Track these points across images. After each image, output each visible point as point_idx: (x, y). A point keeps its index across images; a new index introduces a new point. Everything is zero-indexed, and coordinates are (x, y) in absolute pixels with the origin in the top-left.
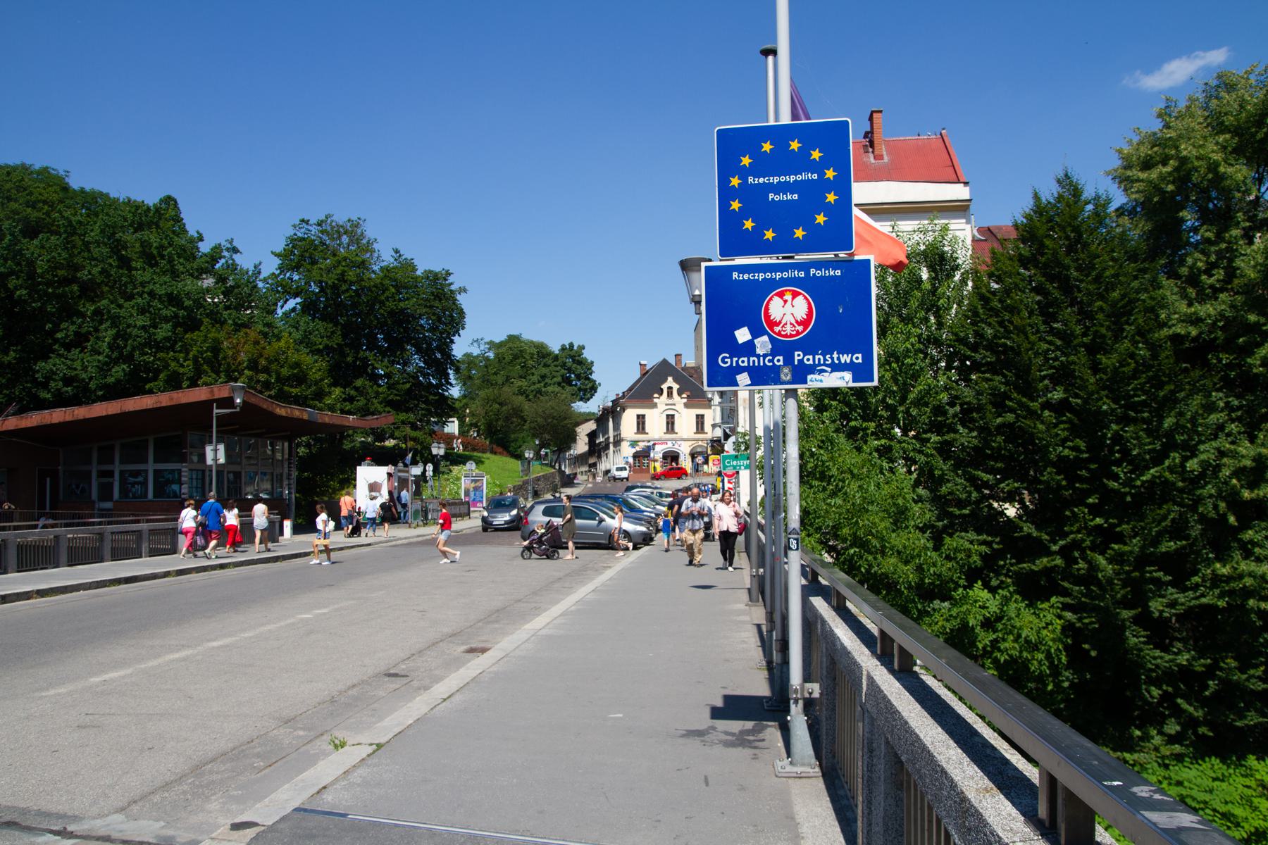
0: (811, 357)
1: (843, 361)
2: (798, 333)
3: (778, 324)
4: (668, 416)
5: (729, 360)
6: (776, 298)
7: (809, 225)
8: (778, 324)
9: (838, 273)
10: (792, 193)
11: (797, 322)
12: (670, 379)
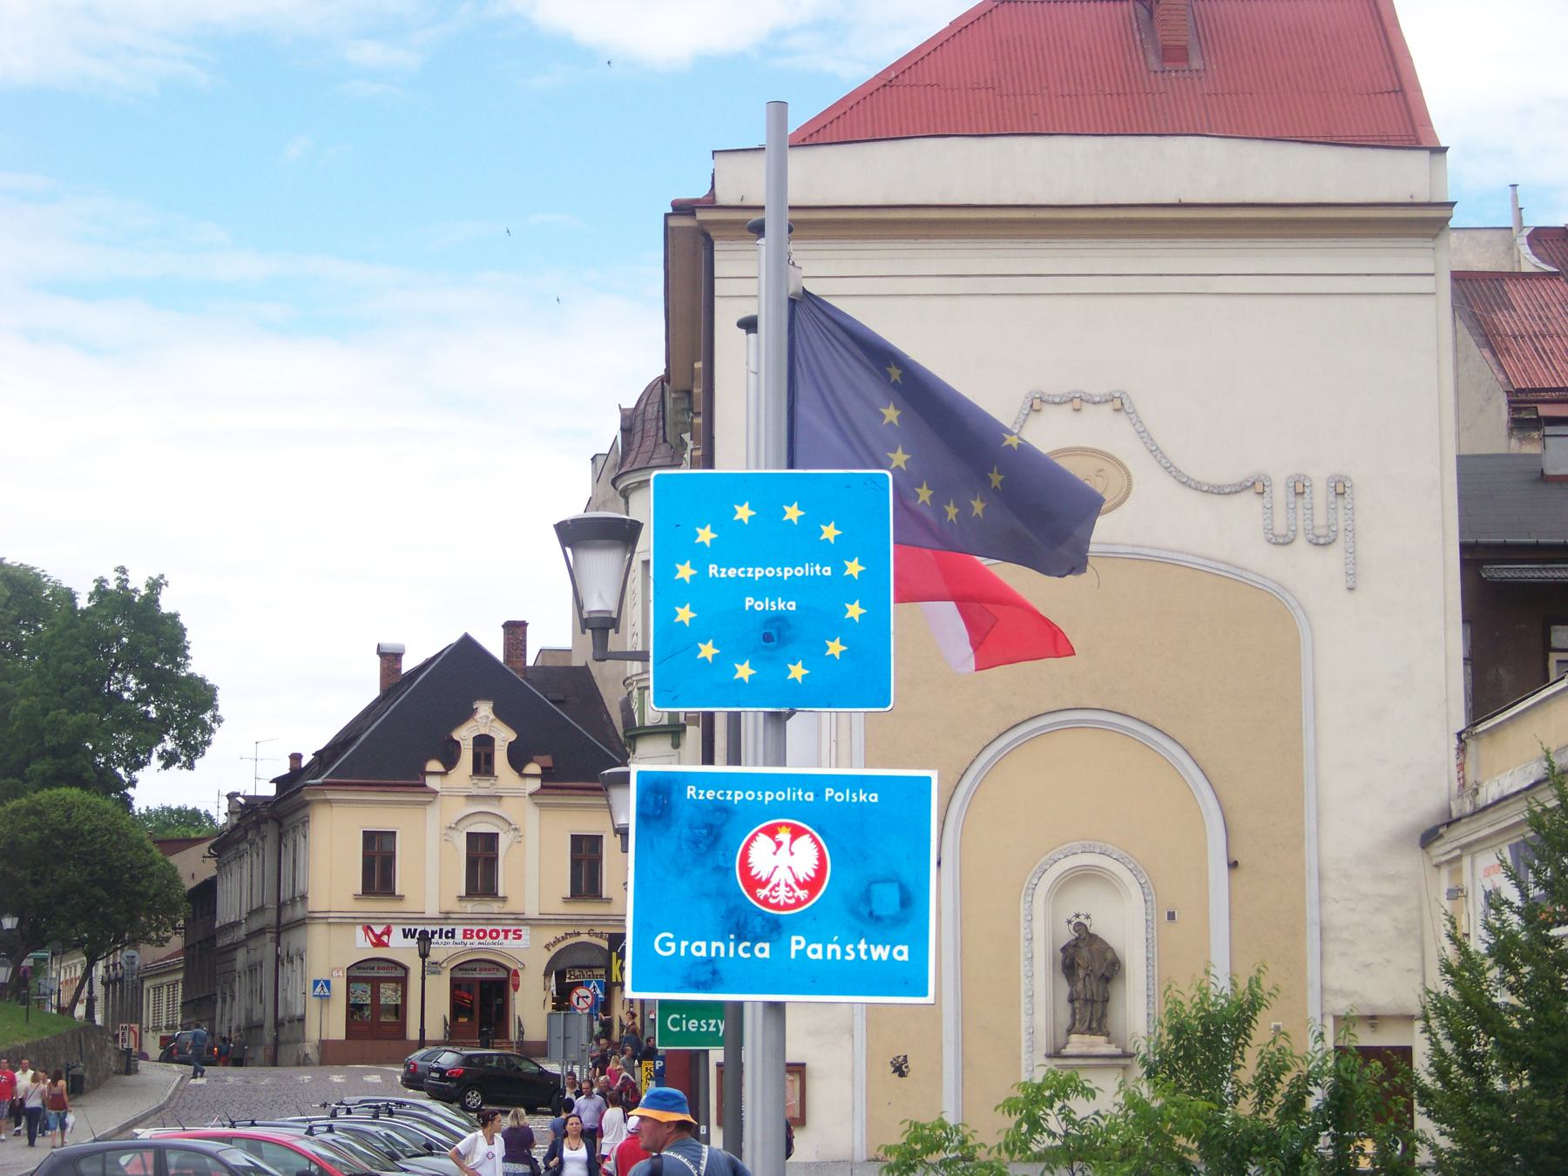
0: (819, 947)
1: (875, 957)
2: (799, 903)
3: (764, 884)
4: (471, 837)
5: (672, 945)
6: (762, 838)
7: (814, 656)
8: (764, 884)
9: (874, 798)
10: (786, 599)
11: (797, 882)
12: (484, 709)
